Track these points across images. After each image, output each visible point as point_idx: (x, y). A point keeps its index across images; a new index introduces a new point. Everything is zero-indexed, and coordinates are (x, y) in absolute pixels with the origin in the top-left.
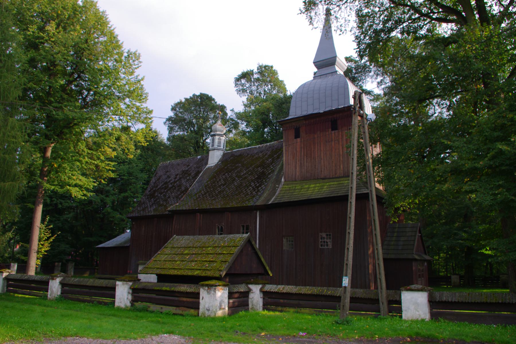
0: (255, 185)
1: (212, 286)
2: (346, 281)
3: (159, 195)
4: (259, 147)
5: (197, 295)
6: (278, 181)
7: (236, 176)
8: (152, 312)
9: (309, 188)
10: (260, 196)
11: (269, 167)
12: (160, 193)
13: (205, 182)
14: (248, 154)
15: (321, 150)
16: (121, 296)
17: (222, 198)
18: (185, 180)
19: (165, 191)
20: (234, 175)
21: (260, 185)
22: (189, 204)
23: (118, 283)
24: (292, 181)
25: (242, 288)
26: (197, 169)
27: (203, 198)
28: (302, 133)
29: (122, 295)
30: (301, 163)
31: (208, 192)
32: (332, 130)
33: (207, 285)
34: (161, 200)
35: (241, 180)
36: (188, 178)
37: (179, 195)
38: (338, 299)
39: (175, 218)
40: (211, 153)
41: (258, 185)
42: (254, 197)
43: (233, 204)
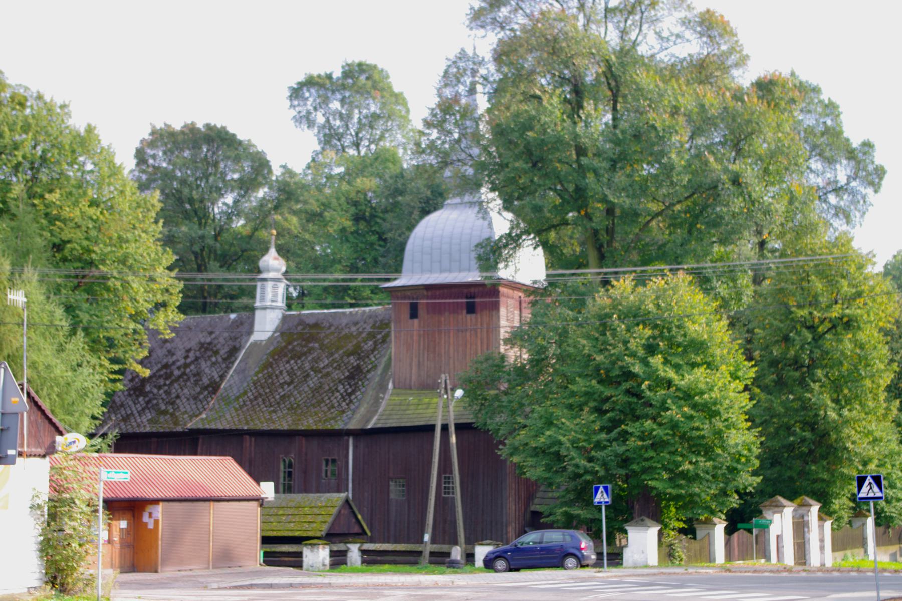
0: (346, 391)
1: (315, 545)
2: (427, 538)
3: (155, 391)
4: (351, 312)
5: (299, 555)
6: (383, 387)
7: (312, 368)
9: (429, 404)
10: (354, 412)
11: (368, 357)
12: (155, 386)
13: (252, 373)
14: (331, 325)
17: (288, 409)
18: (209, 363)
19: (168, 382)
20: (307, 366)
21: (354, 392)
22: (228, 416)
24: (406, 389)
25: (341, 547)
26: (230, 342)
27: (253, 406)
28: (422, 312)
30: (419, 362)
31: (260, 395)
33: (310, 545)
34: (161, 401)
35: (321, 377)
36: (214, 359)
37: (200, 393)
38: (420, 553)
39: (201, 441)
40: (258, 314)
41: (350, 390)
42: (343, 412)
43: (309, 423)
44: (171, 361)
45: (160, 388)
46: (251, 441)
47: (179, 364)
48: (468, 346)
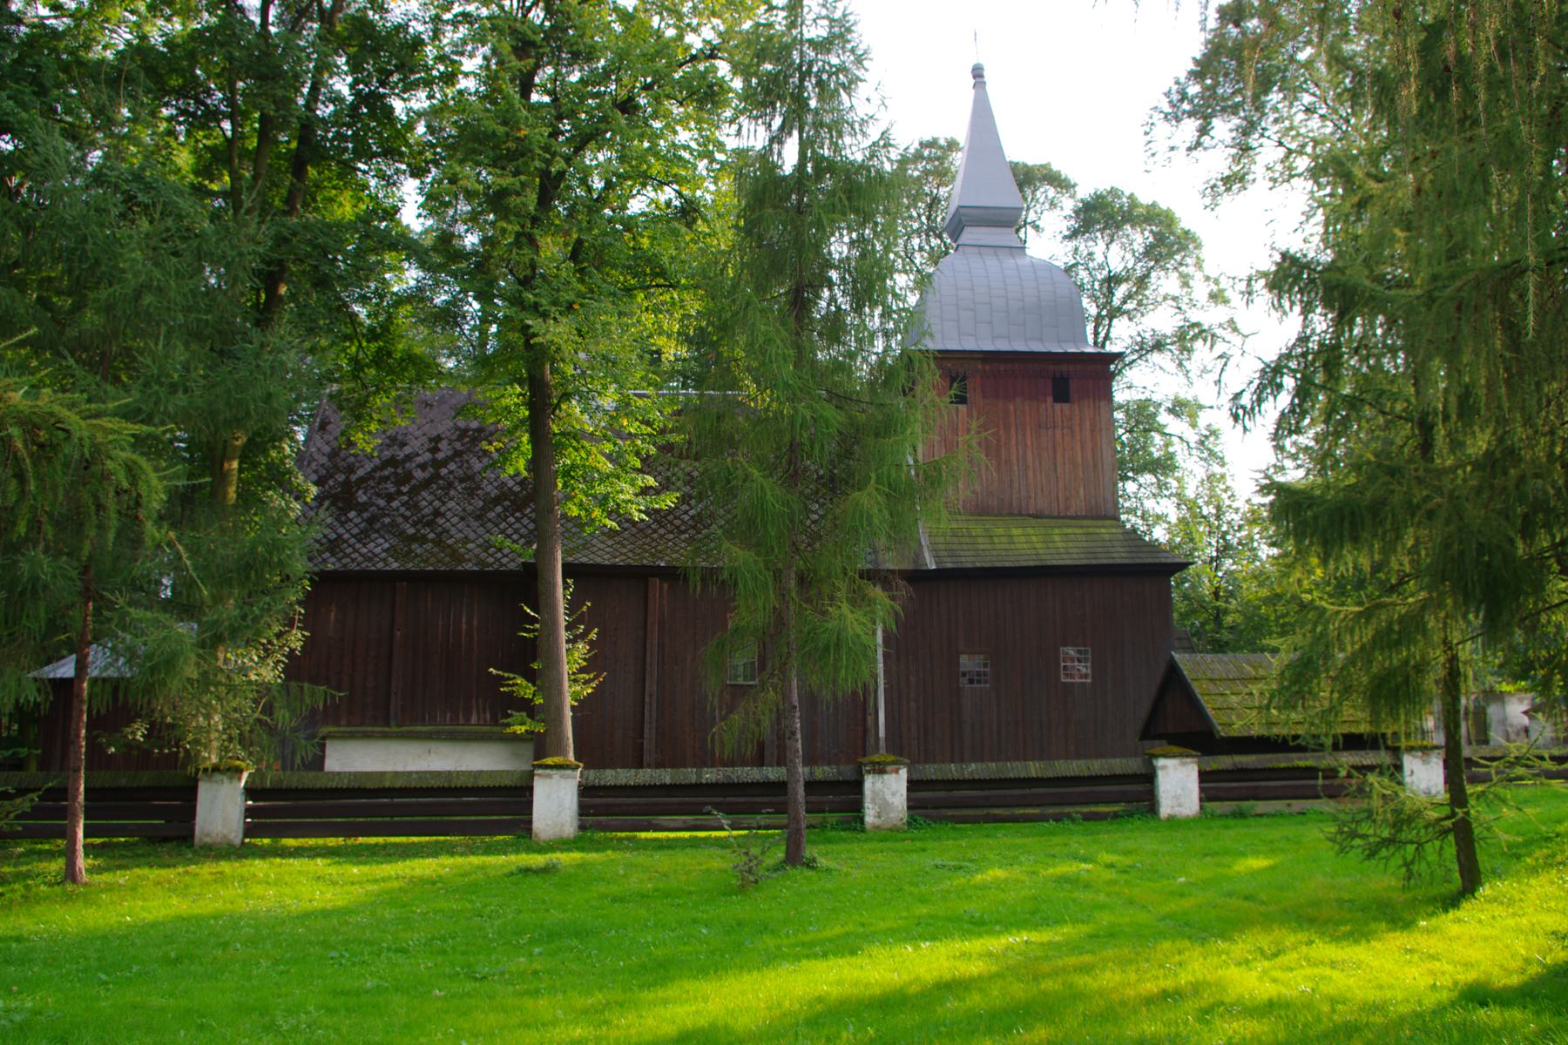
3: (382, 503)
8: (1260, 815)
15: (1026, 446)
16: (1179, 791)
19: (405, 489)
23: (1161, 762)
29: (1183, 789)
32: (1056, 400)
38: (780, 787)
44: (401, 455)
45: (390, 498)
46: (661, 588)
47: (419, 460)
48: (1059, 452)
